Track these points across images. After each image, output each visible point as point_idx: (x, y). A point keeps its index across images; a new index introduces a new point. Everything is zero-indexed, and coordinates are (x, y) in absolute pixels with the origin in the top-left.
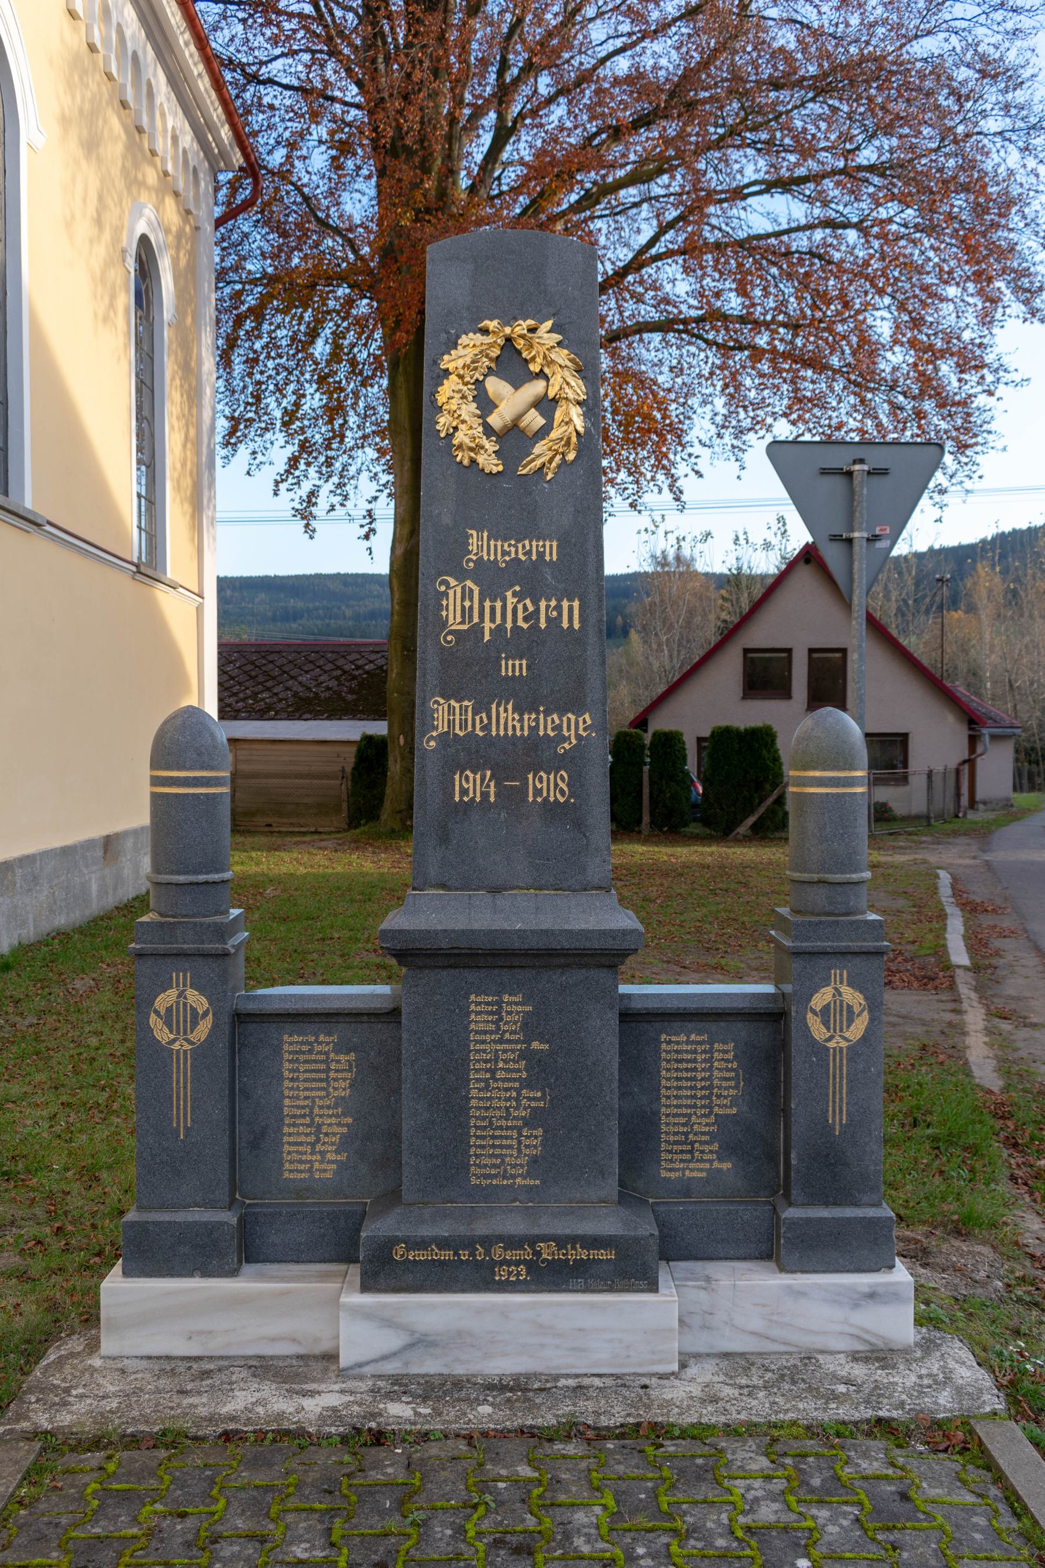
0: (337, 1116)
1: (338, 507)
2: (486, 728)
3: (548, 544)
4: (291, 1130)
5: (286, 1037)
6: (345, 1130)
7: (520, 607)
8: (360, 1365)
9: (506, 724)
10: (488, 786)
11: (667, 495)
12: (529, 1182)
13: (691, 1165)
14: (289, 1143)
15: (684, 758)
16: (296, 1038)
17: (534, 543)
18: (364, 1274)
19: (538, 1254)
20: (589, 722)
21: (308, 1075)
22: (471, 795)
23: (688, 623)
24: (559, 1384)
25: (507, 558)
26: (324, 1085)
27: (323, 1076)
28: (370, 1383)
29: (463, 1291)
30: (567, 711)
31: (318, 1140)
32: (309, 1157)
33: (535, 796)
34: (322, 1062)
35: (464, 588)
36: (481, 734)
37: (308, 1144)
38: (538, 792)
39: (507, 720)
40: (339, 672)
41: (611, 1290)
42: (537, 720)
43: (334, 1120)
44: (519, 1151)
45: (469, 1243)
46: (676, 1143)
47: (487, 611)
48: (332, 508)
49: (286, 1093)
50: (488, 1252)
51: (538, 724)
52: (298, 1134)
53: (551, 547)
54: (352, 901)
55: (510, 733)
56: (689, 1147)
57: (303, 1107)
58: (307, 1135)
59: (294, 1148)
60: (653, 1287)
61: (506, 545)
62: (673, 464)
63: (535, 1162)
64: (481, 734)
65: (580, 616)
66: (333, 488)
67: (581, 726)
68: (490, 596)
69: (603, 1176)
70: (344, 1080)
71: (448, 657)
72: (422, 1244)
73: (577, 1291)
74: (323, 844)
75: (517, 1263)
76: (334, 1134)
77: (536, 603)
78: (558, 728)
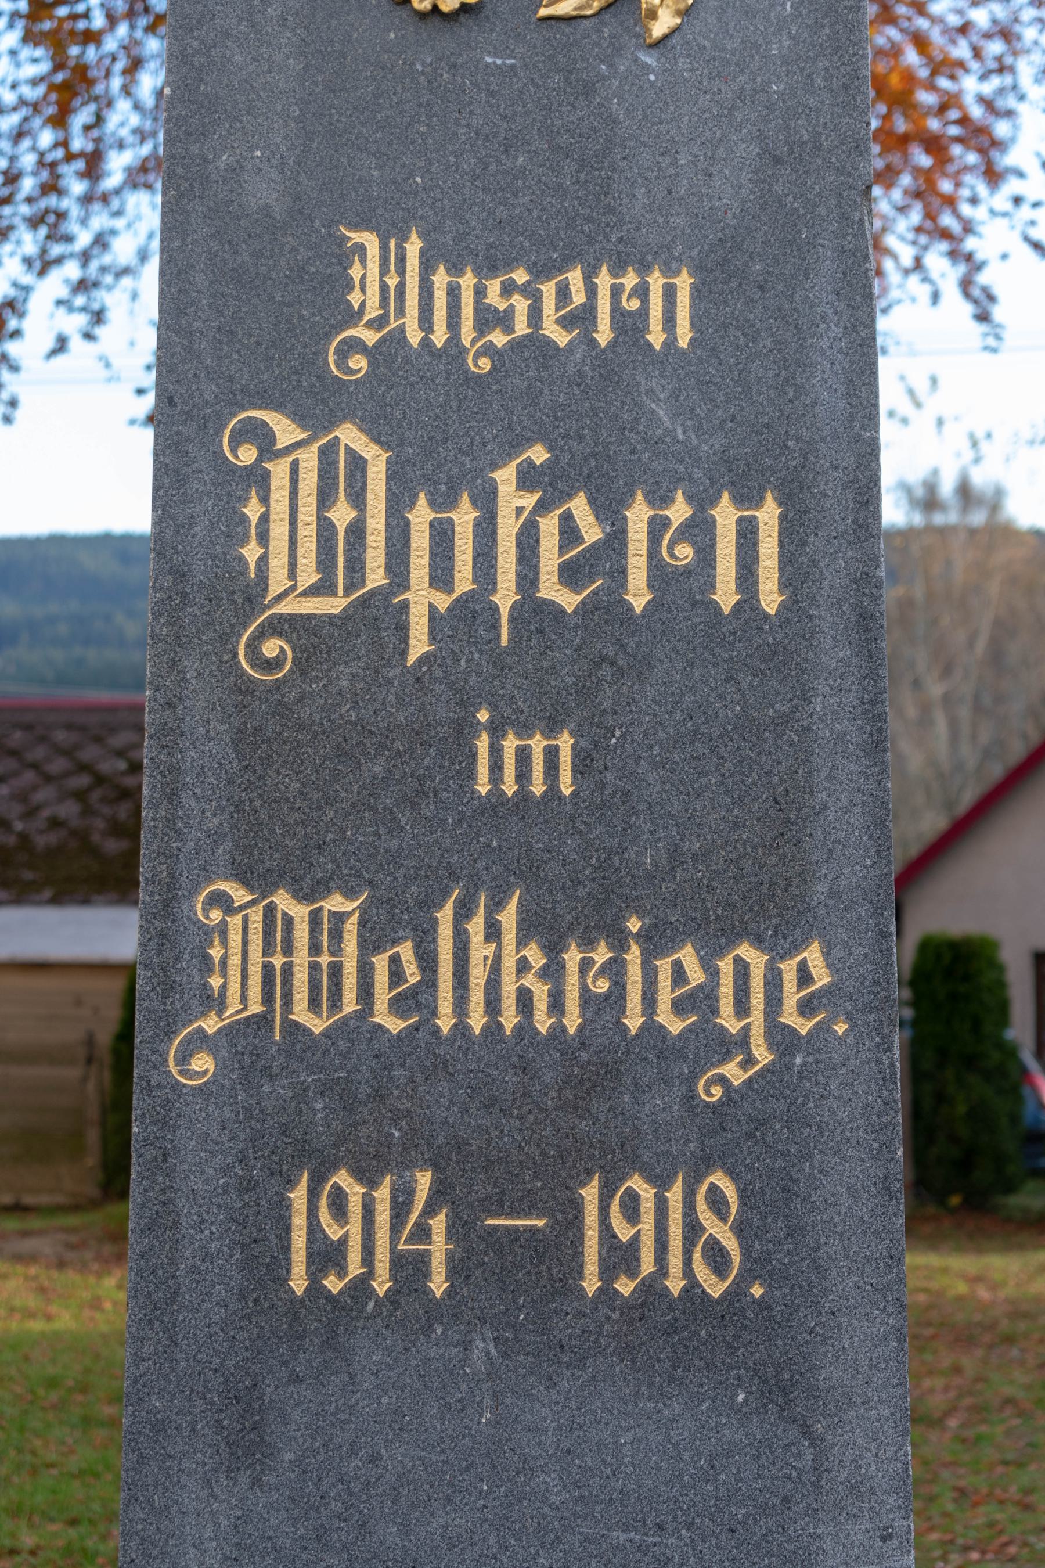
1: (76, 343)
2: (415, 1001)
3: (656, 282)
7: (549, 526)
9: (493, 985)
10: (422, 1233)
11: (957, 308)
15: (1002, 1011)
17: (604, 280)
20: (822, 977)
22: (355, 1268)
23: (996, 656)
25: (499, 339)
30: (732, 936)
33: (608, 1271)
35: (327, 454)
36: (395, 1025)
38: (620, 1257)
39: (497, 972)
40: (83, 781)
42: (615, 969)
47: (420, 542)
48: (61, 345)
51: (619, 987)
53: (670, 293)
54: (87, 1421)
55: (509, 1020)
61: (494, 287)
62: (968, 228)
64: (395, 1025)
65: (786, 560)
66: (64, 292)
67: (791, 995)
68: (430, 482)
71: (264, 726)
74: (29, 1245)
77: (610, 510)
78: (698, 1002)
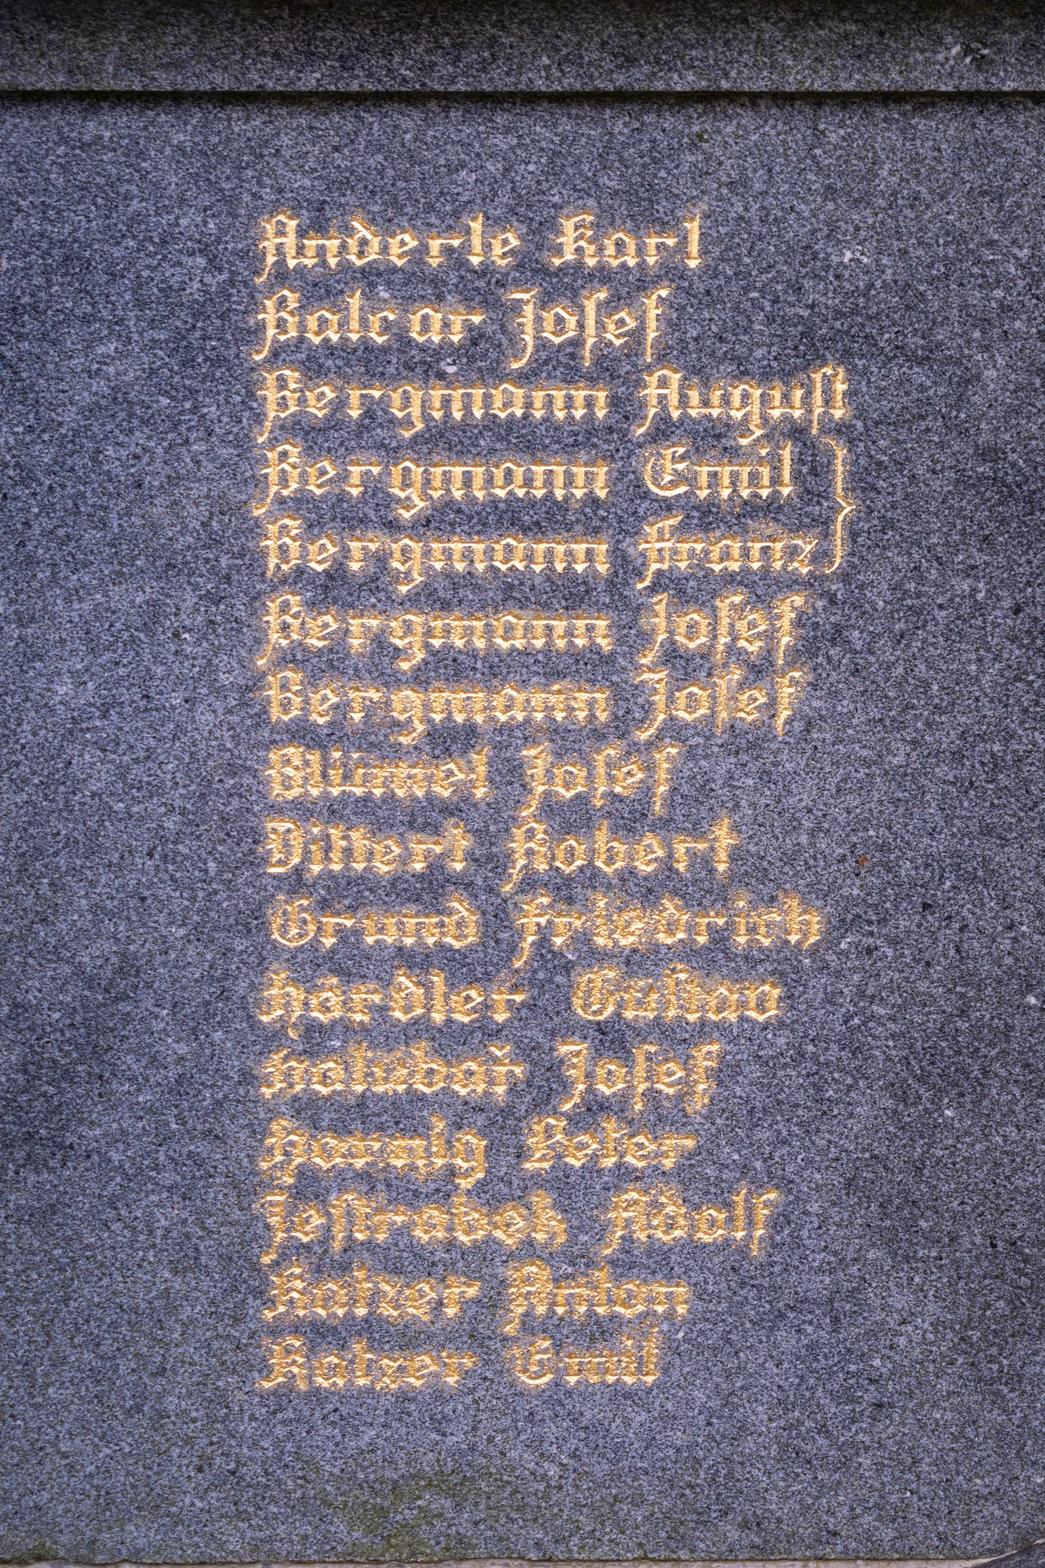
0: (700, 889)
4: (330, 1001)
5: (280, 238)
6: (763, 1001)
14: (309, 1111)
16: (363, 242)
21: (461, 553)
26: (597, 631)
27: (587, 556)
31: (544, 1086)
32: (471, 1225)
34: (576, 440)
37: (464, 1113)
43: (672, 923)
49: (284, 697)
52: (386, 1035)
57: (425, 817)
58: (452, 1041)
59: (355, 1151)
70: (762, 587)
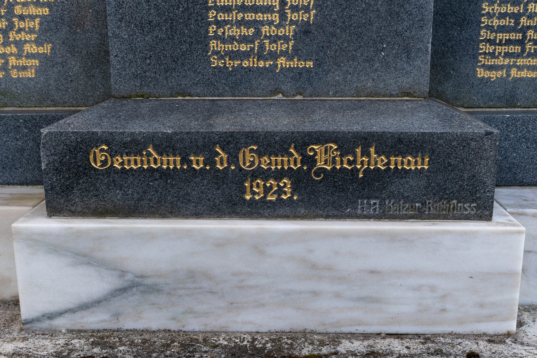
8: (51, 316)
12: (295, 63)
13: (520, 62)
18: (50, 191)
19: (310, 161)
24: (341, 349)
28: (62, 342)
29: (198, 215)
31: (11, 26)
41: (420, 215)
44: (283, 16)
45: (206, 145)
46: (502, 29)
50: (233, 158)
56: (520, 36)
60: (484, 213)
63: (307, 32)
69: (408, 52)
72: (134, 146)
73: (368, 217)
75: (279, 175)
76: (32, 18)
